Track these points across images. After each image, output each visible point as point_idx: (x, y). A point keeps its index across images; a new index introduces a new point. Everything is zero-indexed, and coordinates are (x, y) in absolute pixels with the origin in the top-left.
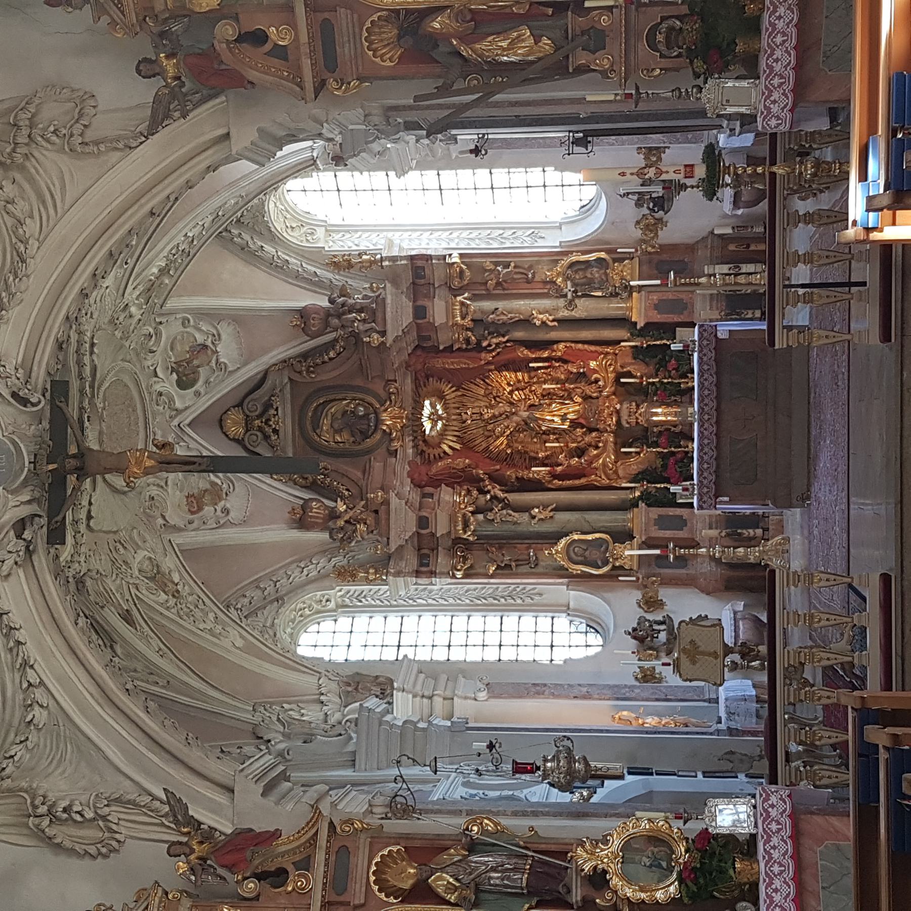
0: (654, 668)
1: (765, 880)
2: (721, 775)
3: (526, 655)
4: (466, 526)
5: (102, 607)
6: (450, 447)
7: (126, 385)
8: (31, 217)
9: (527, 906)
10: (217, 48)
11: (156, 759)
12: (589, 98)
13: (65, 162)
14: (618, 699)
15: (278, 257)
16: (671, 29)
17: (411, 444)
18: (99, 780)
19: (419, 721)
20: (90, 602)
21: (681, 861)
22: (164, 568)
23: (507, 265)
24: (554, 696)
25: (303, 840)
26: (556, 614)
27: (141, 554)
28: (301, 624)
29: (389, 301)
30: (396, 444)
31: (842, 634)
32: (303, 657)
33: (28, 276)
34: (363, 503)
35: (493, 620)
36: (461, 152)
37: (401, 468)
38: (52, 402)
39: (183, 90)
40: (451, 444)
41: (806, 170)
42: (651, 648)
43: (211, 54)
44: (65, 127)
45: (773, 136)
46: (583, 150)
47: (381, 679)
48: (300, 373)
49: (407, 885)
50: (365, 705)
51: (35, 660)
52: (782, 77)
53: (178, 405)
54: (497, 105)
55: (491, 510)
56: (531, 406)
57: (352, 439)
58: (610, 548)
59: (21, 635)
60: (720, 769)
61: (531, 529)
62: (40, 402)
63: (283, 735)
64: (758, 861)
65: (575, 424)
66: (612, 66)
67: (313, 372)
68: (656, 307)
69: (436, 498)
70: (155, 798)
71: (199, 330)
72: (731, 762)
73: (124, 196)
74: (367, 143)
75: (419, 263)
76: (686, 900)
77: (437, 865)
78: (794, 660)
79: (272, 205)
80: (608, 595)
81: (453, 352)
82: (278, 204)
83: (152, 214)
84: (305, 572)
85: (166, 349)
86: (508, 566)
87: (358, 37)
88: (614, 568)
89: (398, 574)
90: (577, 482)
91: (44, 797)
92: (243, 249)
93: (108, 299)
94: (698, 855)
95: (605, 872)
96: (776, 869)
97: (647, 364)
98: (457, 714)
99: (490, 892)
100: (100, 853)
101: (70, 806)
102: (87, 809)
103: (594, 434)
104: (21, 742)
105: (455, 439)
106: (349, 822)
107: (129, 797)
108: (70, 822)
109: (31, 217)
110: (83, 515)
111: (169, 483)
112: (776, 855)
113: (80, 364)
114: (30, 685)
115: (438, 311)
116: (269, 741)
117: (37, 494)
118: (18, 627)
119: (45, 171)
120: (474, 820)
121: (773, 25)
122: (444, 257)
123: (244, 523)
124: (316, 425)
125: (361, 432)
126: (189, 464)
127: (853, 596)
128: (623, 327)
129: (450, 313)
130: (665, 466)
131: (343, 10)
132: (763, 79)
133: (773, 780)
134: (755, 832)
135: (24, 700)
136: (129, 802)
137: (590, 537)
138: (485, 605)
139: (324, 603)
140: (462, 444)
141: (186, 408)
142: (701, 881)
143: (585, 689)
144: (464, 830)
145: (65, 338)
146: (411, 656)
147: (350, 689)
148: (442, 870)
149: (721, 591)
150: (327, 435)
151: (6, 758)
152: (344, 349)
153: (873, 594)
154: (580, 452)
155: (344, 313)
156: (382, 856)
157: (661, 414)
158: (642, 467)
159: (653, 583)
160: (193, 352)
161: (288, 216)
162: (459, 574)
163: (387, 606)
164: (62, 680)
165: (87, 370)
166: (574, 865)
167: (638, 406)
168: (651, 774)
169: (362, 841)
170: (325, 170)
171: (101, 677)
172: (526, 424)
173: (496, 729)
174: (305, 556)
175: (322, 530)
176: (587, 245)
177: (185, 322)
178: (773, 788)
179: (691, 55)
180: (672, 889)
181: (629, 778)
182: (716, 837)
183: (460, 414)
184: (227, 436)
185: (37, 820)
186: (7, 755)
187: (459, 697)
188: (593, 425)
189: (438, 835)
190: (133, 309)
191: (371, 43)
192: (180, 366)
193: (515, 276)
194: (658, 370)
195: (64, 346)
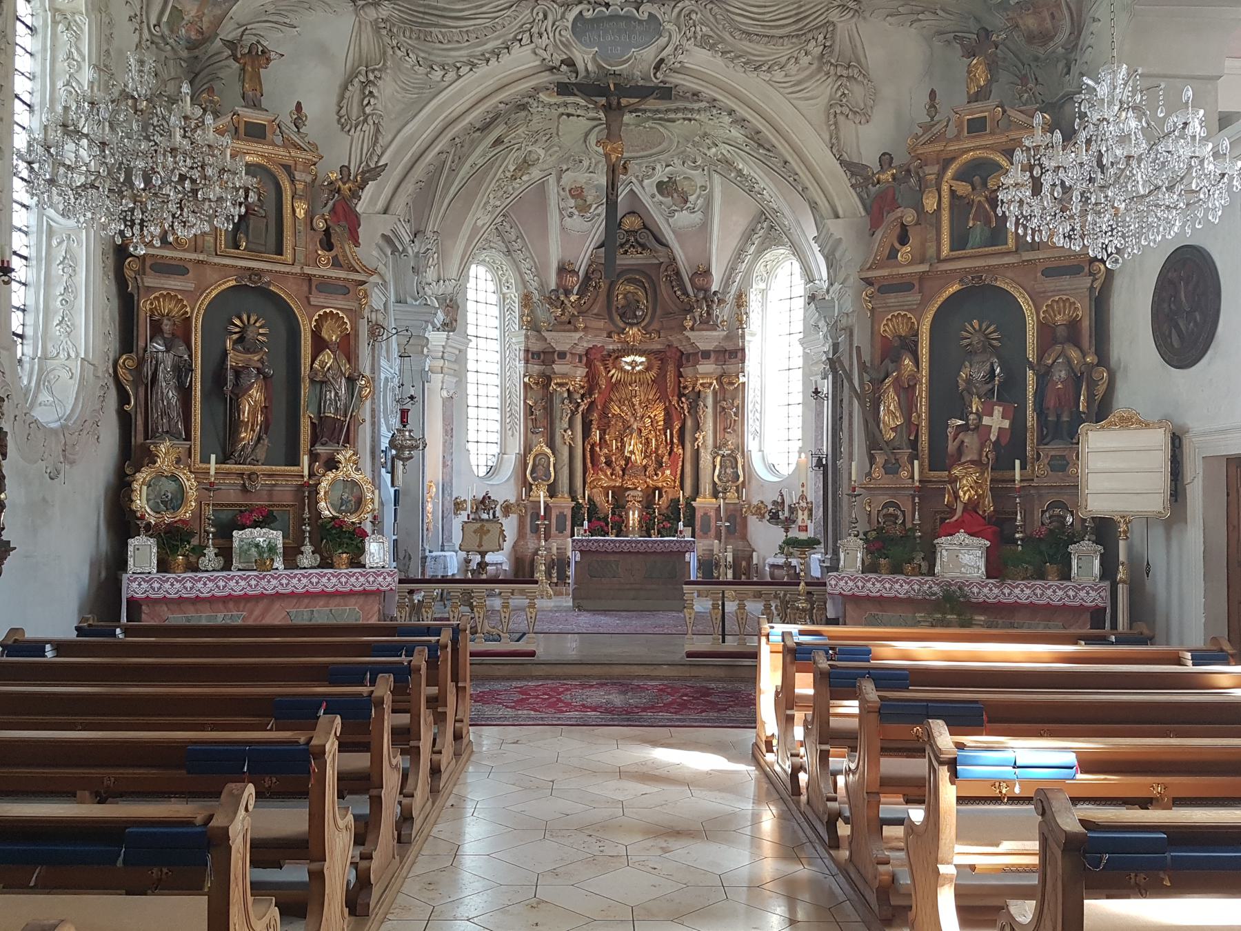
0: (163, 566)
3: (472, 424)
4: (560, 385)
5: (506, 123)
6: (613, 375)
7: (660, 144)
8: (786, 75)
10: (898, 210)
11: (406, 159)
12: (853, 463)
13: (823, 101)
14: (443, 485)
15: (746, 256)
16: (896, 517)
17: (615, 348)
19: (428, 349)
20: (510, 114)
23: (736, 414)
24: (445, 442)
26: (499, 446)
27: (542, 153)
28: (493, 268)
29: (715, 333)
30: (616, 337)
31: (494, 628)
32: (469, 269)
33: (745, 72)
34: (576, 314)
35: (496, 402)
36: (816, 382)
37: (600, 340)
38: (657, 88)
39: (870, 186)
40: (615, 376)
41: (801, 603)
42: (477, 508)
43: (894, 205)
44: (847, 101)
45: (825, 584)
47: (454, 324)
48: (666, 270)
49: (324, 335)
51: (476, 73)
52: (863, 587)
53: (646, 182)
54: (851, 403)
55: (570, 402)
56: (641, 430)
57: (620, 306)
58: (545, 483)
59: (493, 61)
60: (399, 550)
61: (557, 430)
62: (656, 78)
63: (418, 252)
65: (628, 460)
66: (874, 479)
67: (666, 279)
68: (706, 514)
69: (579, 364)
70: (380, 157)
71: (698, 198)
73: (798, 142)
74: (825, 317)
75: (739, 354)
76: (320, 521)
79: (782, 251)
80: (512, 481)
81: (679, 377)
82: (783, 256)
83: (786, 162)
84: (528, 272)
85: (686, 174)
86: (532, 413)
87: (899, 308)
89: (527, 337)
90: (588, 461)
91: (380, 78)
92: (753, 230)
93: (722, 131)
94: (351, 529)
95: (337, 469)
97: (667, 508)
98: (433, 376)
99: (321, 392)
100: (341, 117)
103: (621, 472)
104: (418, 62)
105: (619, 378)
106: (366, 296)
107: (380, 138)
109: (786, 75)
110: (570, 110)
111: (592, 174)
112: (353, 579)
113: (676, 110)
114: (458, 69)
115: (706, 367)
116: (413, 242)
118: (499, 60)
119: (817, 86)
122: (743, 372)
123: (563, 228)
124: (629, 281)
125: (624, 313)
126: (612, 186)
127: (518, 636)
128: (692, 492)
129: (705, 375)
130: (599, 519)
131: (920, 297)
132: (862, 575)
133: (401, 581)
135: (448, 64)
136: (377, 139)
137: (552, 469)
138: (505, 397)
139: (506, 284)
140: (615, 384)
141: (643, 188)
142: (334, 531)
143: (449, 463)
145: (701, 98)
146: (471, 345)
147: (448, 301)
148: (335, 359)
149: (515, 555)
150: (622, 289)
151: (407, 51)
152: (682, 302)
153: (521, 646)
154: (609, 463)
155: (706, 302)
157: (634, 517)
158: (598, 505)
159: (521, 510)
160: (683, 193)
161: (774, 263)
162: (526, 380)
163: (504, 329)
165: (672, 116)
167: (639, 502)
168: (395, 505)
169: (353, 304)
170: (805, 289)
171: (464, 120)
172: (629, 427)
173: (423, 402)
174: (539, 271)
175: (557, 284)
176: (748, 467)
177: (703, 188)
178: (397, 579)
179: (879, 530)
180: (327, 512)
181: (392, 490)
182: (362, 542)
183: (635, 382)
184: (623, 217)
185: (364, 72)
187: (443, 377)
188: (627, 472)
190: (714, 150)
191: (897, 317)
192: (673, 184)
193: (729, 421)
194: (663, 515)
195: (695, 98)
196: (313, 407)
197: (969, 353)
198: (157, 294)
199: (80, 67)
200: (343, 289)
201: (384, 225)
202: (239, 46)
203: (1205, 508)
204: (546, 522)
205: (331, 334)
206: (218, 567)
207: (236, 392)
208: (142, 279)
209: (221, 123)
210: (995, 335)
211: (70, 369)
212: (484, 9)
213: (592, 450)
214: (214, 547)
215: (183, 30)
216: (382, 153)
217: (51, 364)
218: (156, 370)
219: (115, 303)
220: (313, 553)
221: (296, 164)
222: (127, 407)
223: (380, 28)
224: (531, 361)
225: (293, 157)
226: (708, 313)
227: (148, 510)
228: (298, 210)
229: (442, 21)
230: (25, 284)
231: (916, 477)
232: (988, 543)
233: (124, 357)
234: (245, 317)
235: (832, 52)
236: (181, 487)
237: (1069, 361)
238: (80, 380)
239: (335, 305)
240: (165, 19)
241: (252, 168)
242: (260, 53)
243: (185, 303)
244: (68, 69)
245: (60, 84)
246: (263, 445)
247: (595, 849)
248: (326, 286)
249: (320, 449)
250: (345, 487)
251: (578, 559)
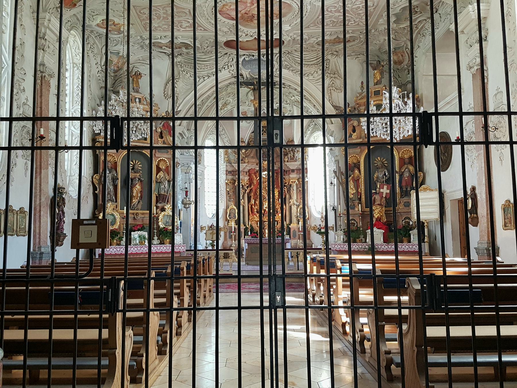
11: (187, 108)
16: (355, 224)
22: (228, 106)
27: (231, 100)
29: (296, 163)
46: (332, 209)
49: (160, 166)
68: (294, 230)
70: (178, 107)
83: (314, 106)
88: (229, 220)
89: (227, 166)
90: (250, 211)
95: (165, 211)
99: (159, 186)
115: (293, 176)
117: (249, 79)
128: (289, 222)
129: (293, 178)
130: (254, 233)
158: (254, 228)
164: (205, 86)
190: (293, 98)
191: (353, 157)
196: (157, 191)
197: (377, 168)
203: (451, 217)
204: (235, 234)
205: (162, 166)
210: (386, 162)
212: (212, 58)
213: (251, 207)
216: (179, 106)
219: (92, 158)
220: (158, 239)
222: (96, 192)
224: (228, 174)
226: (293, 156)
231: (360, 210)
232: (384, 231)
234: (134, 161)
235: (329, 69)
236: (115, 218)
237: (409, 171)
245: (75, 87)
247: (253, 314)
249: (159, 205)
251: (247, 248)
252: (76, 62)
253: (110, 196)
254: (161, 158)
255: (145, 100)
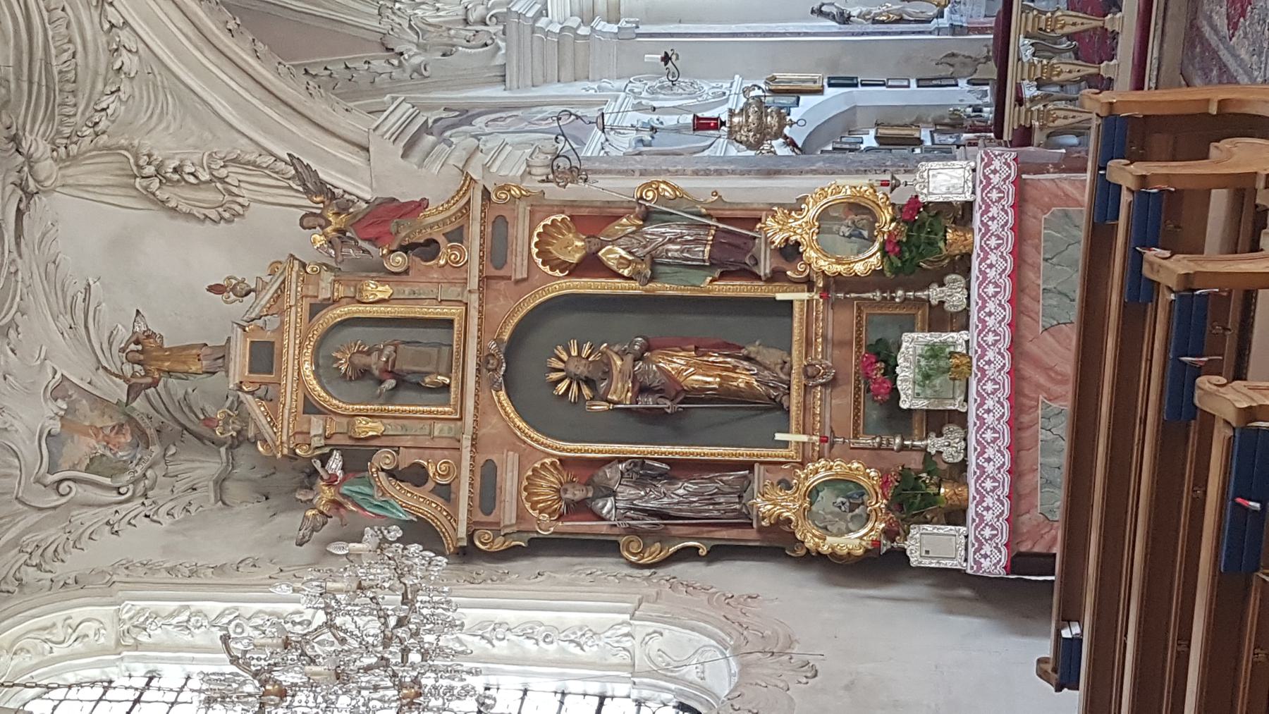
0: (956, 516)
1: (976, 449)
2: (938, 82)
9: (709, 279)
18: (210, 137)
21: (885, 229)
25: (454, 209)
49: (575, 258)
50: (513, 9)
60: (937, 75)
63: (418, 45)
64: (972, 230)
70: (277, 159)
72: (952, 65)
77: (608, 236)
78: (1033, 27)
91: (150, 156)
96: (993, 242)
99: (668, 265)
100: (222, 218)
101: (181, 166)
102: (201, 170)
104: (112, 93)
106: (505, 188)
107: (248, 157)
108: (183, 183)
112: (993, 226)
114: (113, 26)
116: (402, 54)
120: (649, 185)
121: (981, 516)
134: (971, 199)
135: (108, 44)
136: (248, 163)
144: (638, 199)
148: (613, 242)
151: (96, 111)
156: (544, 226)
164: (149, 20)
166: (763, 237)
168: (856, 85)
169: (521, 210)
171: (196, 14)
181: (830, 92)
185: (145, 182)
186: (98, 108)
189: (608, 202)
196: (694, 276)
198: (528, 505)
199: (198, 613)
200: (499, 228)
201: (387, 154)
202: (134, 380)
205: (574, 248)
206: (959, 433)
207: (673, 393)
208: (506, 527)
209: (256, 408)
211: (648, 635)
214: (927, 437)
215: (120, 454)
216: (272, 154)
217: (642, 662)
218: (643, 510)
220: (942, 284)
221: (307, 296)
222: (703, 552)
223: (68, 155)
225: (297, 301)
227: (863, 532)
228: (380, 296)
229: (39, 53)
230: (525, 692)
233: (625, 554)
234: (555, 376)
238: (665, 623)
239: (523, 239)
240: (107, 481)
241: (321, 362)
242: (140, 347)
243: (537, 465)
244: (203, 629)
246: (758, 353)
248: (497, 252)
249: (765, 268)
250: (830, 232)
252: (114, 636)
253: (724, 494)
254: (535, 250)
255: (260, 323)
